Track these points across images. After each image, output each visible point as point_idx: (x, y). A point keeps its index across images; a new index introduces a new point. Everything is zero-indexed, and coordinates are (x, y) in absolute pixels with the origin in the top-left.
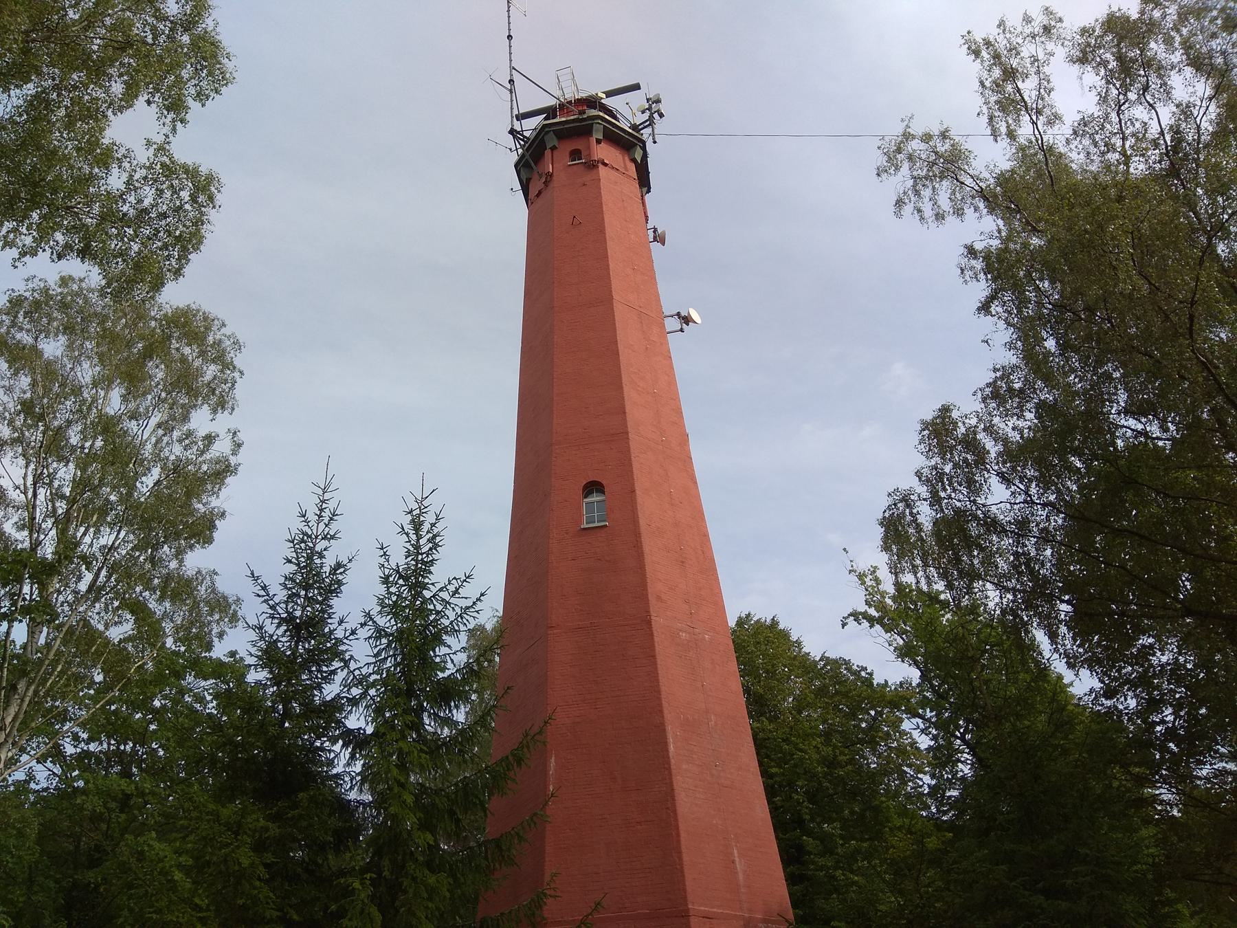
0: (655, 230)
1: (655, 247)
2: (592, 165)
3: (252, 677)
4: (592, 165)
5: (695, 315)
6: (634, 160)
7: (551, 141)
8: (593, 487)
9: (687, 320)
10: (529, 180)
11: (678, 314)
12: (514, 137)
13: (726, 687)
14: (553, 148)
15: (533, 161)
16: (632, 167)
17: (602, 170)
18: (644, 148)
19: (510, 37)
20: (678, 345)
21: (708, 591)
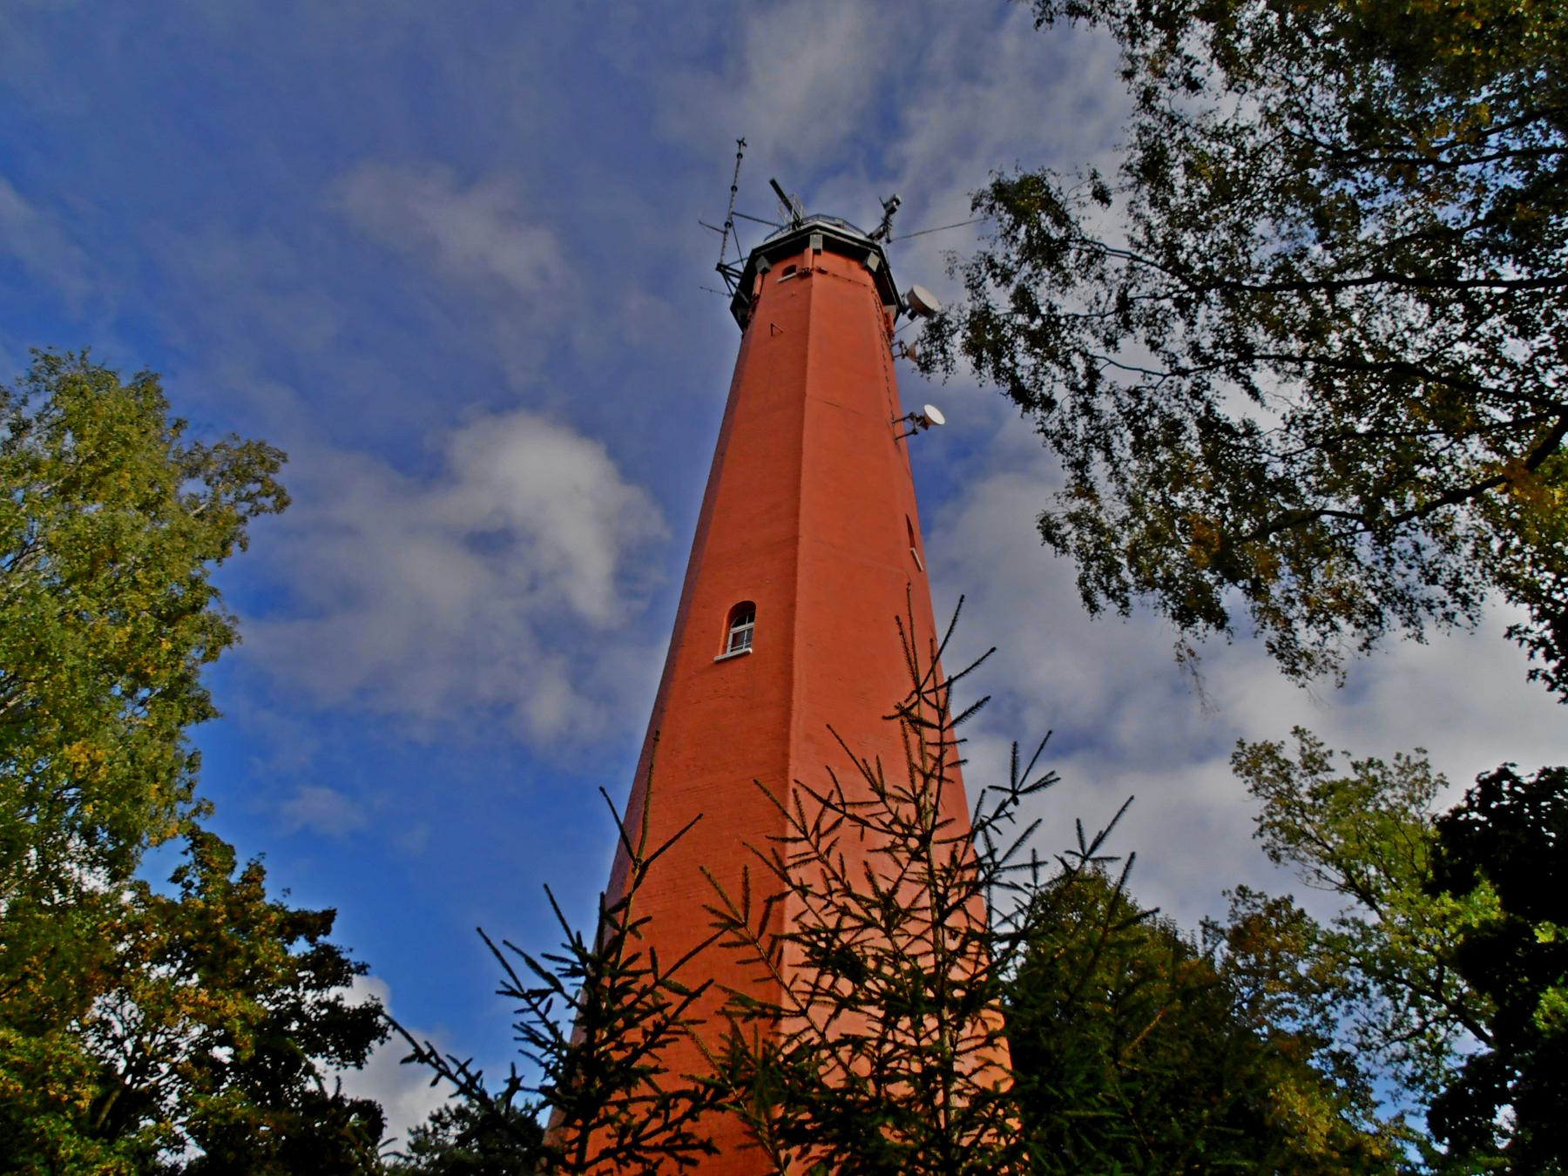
4: (806, 274)
7: (763, 263)
11: (912, 416)
14: (765, 272)
17: (816, 277)
18: (880, 254)
19: (734, 188)
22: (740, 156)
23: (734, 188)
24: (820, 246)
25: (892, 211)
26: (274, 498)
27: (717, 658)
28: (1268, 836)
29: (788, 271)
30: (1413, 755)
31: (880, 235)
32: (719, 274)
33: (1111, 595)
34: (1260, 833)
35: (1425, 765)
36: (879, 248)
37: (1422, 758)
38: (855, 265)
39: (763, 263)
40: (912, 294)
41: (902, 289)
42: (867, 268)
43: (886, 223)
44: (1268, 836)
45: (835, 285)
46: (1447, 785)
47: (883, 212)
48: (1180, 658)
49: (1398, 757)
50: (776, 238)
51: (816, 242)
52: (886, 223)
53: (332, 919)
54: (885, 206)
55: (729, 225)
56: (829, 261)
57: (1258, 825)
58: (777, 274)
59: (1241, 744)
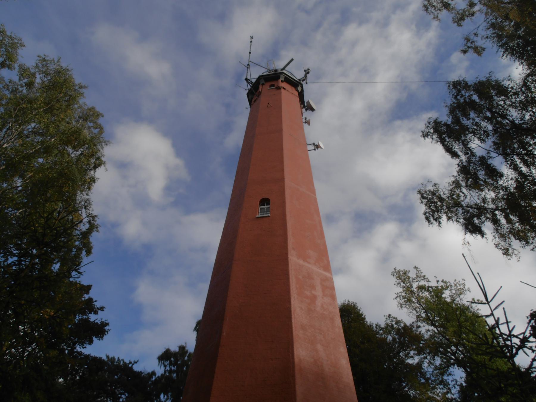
0: (306, 118)
1: (306, 125)
2: (279, 88)
3: (85, 295)
4: (279, 88)
5: (321, 145)
6: (297, 91)
7: (262, 81)
8: (265, 201)
9: (317, 147)
10: (252, 99)
11: (314, 144)
12: (247, 82)
13: (338, 359)
14: (263, 84)
15: (254, 93)
16: (297, 93)
17: (282, 90)
18: (302, 87)
19: (250, 53)
20: (313, 155)
21: (329, 289)
22: (251, 42)
23: (250, 53)
24: (283, 79)
25: (308, 73)
26: (99, 130)
27: (257, 216)
28: (398, 299)
29: (271, 86)
30: (461, 280)
31: (303, 81)
32: (246, 82)
33: (435, 220)
34: (396, 298)
35: (464, 284)
36: (302, 85)
37: (463, 282)
38: (293, 89)
39: (262, 81)
40: (308, 102)
41: (306, 100)
42: (297, 91)
43: (306, 76)
44: (398, 299)
45: (288, 95)
46: (470, 292)
47: (304, 73)
48: (464, 244)
49: (455, 280)
50: (265, 74)
51: (282, 78)
52: (306, 76)
53: (90, 289)
54: (305, 71)
55: (248, 65)
56: (284, 85)
57: (396, 296)
58: (267, 86)
59: (395, 269)
